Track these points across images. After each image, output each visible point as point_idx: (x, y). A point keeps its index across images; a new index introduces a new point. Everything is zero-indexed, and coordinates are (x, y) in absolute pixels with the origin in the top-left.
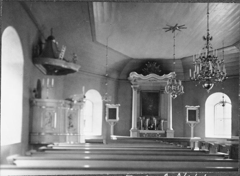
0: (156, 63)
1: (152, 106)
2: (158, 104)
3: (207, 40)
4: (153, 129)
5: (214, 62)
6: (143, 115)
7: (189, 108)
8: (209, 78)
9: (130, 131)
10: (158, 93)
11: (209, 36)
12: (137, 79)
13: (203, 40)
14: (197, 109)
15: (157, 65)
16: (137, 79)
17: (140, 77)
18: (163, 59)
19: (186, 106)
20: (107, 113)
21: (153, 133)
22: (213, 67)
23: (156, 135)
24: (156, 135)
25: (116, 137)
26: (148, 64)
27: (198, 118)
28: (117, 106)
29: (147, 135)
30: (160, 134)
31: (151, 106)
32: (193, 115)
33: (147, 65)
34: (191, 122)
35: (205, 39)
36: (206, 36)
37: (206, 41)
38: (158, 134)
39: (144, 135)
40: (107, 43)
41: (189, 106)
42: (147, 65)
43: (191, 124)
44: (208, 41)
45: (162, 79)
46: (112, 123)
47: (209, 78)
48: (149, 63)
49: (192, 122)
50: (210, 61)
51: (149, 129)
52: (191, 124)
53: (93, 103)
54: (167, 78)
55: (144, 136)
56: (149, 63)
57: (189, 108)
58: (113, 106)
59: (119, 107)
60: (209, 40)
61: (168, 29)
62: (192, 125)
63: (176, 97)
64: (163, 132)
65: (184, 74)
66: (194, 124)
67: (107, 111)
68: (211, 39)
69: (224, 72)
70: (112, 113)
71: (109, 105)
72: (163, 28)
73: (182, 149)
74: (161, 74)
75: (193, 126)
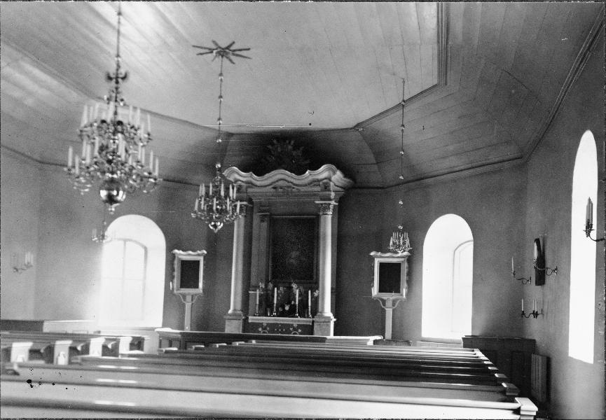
0: (292, 142)
1: (298, 253)
2: (313, 248)
3: (114, 80)
4: (291, 313)
5: (131, 140)
6: (274, 277)
7: (379, 259)
8: (115, 176)
9: (335, 320)
10: (314, 219)
11: (119, 72)
12: (243, 184)
13: (104, 81)
14: (403, 259)
15: (296, 147)
16: (243, 184)
17: (249, 179)
18: (308, 131)
19: (372, 254)
20: (177, 274)
21: (282, 324)
22: (127, 151)
23: (291, 329)
24: (291, 329)
25: (181, 333)
26: (273, 145)
27: (406, 285)
28: (199, 255)
29: (268, 329)
30: (299, 326)
31: (294, 254)
32: (391, 277)
33: (270, 147)
34: (385, 296)
35: (110, 78)
36: (112, 72)
37: (113, 83)
38: (295, 325)
39: (260, 329)
40: (117, 88)
41: (379, 254)
42: (270, 147)
43: (384, 302)
44: (117, 82)
45: (306, 181)
46: (189, 298)
47: (115, 176)
48: (275, 141)
49: (389, 297)
50: (120, 135)
51: (283, 314)
52: (384, 302)
53: (146, 249)
54: (319, 181)
55: (260, 332)
56: (275, 141)
57: (379, 259)
58: (189, 255)
59: (205, 257)
60: (120, 80)
61: (207, 51)
62: (389, 304)
63: (220, 227)
64: (307, 321)
65: (379, 168)
66: (394, 302)
67: (177, 266)
68: (124, 78)
69: (139, 157)
70: (188, 274)
71: (181, 252)
72: (215, 40)
73: (194, 355)
74: (300, 171)
75: (391, 305)
